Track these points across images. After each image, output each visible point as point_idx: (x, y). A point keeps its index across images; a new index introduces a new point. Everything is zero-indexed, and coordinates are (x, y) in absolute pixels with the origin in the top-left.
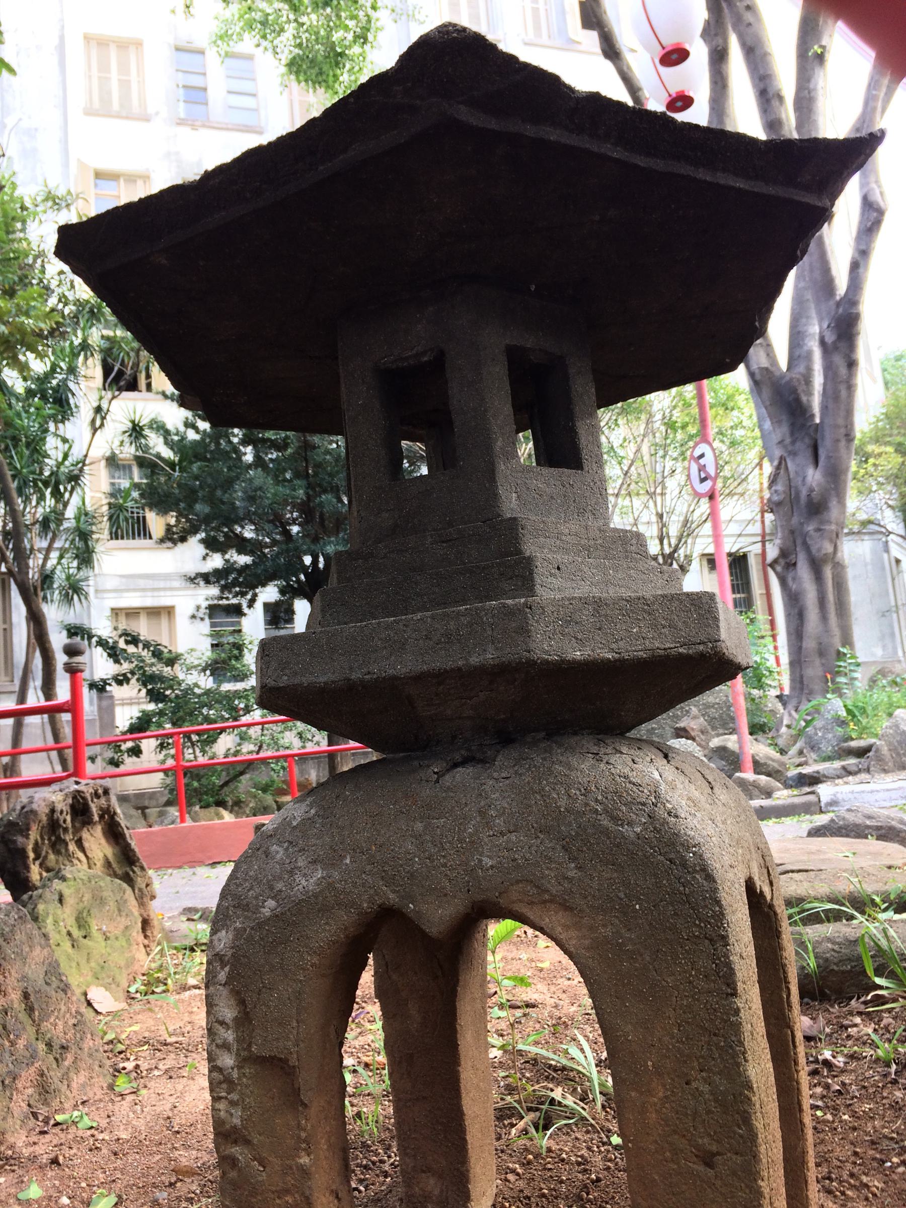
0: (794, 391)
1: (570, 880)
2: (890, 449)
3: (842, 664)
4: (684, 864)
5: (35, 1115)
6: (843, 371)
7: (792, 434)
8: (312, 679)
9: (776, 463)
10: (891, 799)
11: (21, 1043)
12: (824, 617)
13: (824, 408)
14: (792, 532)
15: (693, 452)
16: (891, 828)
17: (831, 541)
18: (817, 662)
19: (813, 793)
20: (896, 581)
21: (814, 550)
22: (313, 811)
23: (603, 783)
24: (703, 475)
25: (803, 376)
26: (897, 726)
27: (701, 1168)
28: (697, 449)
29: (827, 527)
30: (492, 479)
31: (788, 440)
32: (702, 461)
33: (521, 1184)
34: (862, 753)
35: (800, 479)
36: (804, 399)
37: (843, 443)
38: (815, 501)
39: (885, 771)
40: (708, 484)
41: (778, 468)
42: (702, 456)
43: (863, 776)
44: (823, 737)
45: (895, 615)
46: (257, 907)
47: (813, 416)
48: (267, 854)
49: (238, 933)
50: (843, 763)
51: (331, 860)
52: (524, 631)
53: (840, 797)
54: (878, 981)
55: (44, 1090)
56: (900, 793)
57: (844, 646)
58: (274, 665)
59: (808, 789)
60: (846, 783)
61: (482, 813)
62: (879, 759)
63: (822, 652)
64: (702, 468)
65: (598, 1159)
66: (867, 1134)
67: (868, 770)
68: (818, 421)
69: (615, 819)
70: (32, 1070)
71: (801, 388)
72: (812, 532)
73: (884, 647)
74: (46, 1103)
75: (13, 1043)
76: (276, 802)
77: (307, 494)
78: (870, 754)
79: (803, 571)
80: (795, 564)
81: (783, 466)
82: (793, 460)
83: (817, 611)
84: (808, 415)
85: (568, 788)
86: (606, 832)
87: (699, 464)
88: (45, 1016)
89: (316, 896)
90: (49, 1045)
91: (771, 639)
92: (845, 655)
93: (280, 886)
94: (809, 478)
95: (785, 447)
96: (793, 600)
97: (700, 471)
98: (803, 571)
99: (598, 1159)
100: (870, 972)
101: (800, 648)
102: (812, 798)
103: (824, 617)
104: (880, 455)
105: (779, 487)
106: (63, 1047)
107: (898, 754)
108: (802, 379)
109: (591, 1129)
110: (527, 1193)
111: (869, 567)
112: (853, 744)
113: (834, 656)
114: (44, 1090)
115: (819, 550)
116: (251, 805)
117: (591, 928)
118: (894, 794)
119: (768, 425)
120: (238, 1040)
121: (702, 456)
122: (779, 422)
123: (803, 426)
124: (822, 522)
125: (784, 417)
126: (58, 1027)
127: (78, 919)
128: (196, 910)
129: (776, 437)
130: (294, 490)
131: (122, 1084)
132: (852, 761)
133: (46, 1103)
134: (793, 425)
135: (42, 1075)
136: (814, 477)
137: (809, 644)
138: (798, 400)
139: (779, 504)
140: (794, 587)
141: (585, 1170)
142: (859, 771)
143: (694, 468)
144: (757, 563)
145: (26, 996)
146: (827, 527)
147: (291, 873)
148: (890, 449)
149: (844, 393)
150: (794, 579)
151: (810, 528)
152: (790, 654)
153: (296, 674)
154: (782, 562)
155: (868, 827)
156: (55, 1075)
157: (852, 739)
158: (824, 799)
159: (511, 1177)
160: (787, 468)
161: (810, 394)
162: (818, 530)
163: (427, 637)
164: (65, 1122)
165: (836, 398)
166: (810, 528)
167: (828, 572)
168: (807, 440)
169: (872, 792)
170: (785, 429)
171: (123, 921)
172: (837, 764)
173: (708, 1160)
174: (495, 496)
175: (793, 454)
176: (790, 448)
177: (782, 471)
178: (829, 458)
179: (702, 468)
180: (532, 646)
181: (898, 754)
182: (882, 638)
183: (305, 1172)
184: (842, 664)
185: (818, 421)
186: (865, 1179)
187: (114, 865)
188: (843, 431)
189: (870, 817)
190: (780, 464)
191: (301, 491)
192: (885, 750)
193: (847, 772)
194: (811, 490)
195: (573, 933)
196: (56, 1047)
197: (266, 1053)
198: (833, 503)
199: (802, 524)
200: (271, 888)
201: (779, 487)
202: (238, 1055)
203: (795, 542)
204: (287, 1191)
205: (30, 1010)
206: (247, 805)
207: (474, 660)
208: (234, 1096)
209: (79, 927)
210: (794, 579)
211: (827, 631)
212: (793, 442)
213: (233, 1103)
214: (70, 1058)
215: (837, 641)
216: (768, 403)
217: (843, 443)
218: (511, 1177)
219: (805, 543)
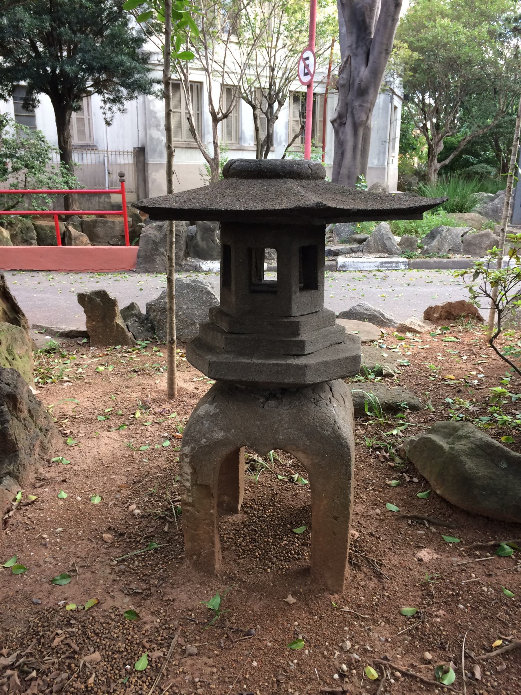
0: (363, 15)
1: (307, 445)
2: (406, 45)
3: (359, 185)
4: (342, 445)
5: (43, 459)
6: (392, 8)
7: (357, 43)
8: (227, 378)
9: (345, 59)
10: (370, 267)
11: (32, 431)
12: (354, 157)
13: (377, 30)
14: (347, 104)
15: (302, 54)
16: (375, 316)
17: (366, 113)
18: (346, 181)
19: (334, 260)
20: (392, 125)
21: (356, 117)
22: (218, 410)
23: (319, 416)
24: (306, 71)
25: (369, 4)
26: (380, 231)
27: (333, 520)
28: (305, 53)
29: (365, 105)
30: (290, 302)
31: (354, 46)
32: (307, 62)
33: (251, 494)
34: (361, 241)
35: (356, 72)
36: (367, 20)
37: (383, 55)
38: (362, 88)
39: (370, 253)
40: (308, 78)
41: (346, 63)
42: (307, 59)
43: (360, 254)
44: (344, 230)
45: (387, 144)
46: (199, 441)
47: (370, 33)
48: (202, 424)
49: (193, 449)
50: (351, 246)
51: (227, 429)
52: (304, 374)
53: (347, 263)
54: (368, 413)
55: (43, 448)
56: (375, 264)
57: (361, 175)
58: (213, 371)
59: (332, 258)
60: (351, 257)
61: (280, 421)
62: (368, 246)
63: (349, 177)
64: (306, 66)
65: (275, 485)
66: (361, 476)
67: (362, 251)
68: (372, 37)
69: (322, 429)
70: (38, 441)
71: (367, 13)
72: (357, 107)
73: (379, 159)
74: (45, 453)
75: (29, 432)
76: (33, 224)
77: (51, 25)
78: (365, 243)
79: (348, 128)
80: (345, 124)
81: (349, 62)
82: (355, 59)
83: (351, 153)
84: (368, 32)
85: (308, 416)
86: (320, 433)
87: (305, 63)
88: (38, 418)
89: (221, 440)
90: (41, 429)
91: (321, 149)
92: (361, 180)
93: (208, 435)
94: (361, 73)
95: (352, 50)
96: (340, 144)
97: (305, 68)
98: (348, 128)
99: (275, 485)
100: (366, 410)
101: (339, 172)
102: (334, 263)
103: (354, 157)
104: (400, 48)
105: (344, 75)
106: (46, 430)
107: (378, 245)
108: (368, 7)
109: (271, 473)
110: (254, 497)
111: (381, 111)
112: (358, 236)
113: (355, 179)
114: (43, 448)
115: (359, 118)
116: (19, 226)
117: (312, 460)
118: (372, 265)
119: (344, 30)
120: (192, 479)
121: (307, 59)
122: (352, 33)
123: (364, 38)
124: (363, 101)
125: (354, 31)
126: (41, 422)
127: (8, 350)
128: (42, 328)
129: (348, 43)
130: (43, 22)
131: (70, 441)
132: (355, 246)
133: (45, 453)
134: (358, 37)
135: (42, 442)
136: (364, 72)
137: (344, 171)
138: (364, 21)
139: (343, 86)
140: (342, 137)
141: (272, 490)
142: (358, 251)
143: (302, 65)
144: (321, 102)
145: (29, 411)
146: (365, 105)
147: (212, 432)
148: (406, 45)
149: (390, 23)
150: (343, 132)
151: (357, 104)
152: (333, 175)
153: (221, 375)
154: (338, 121)
155: (365, 314)
156: (46, 441)
157: (357, 233)
158: (339, 264)
159: (247, 492)
160: (351, 64)
161: (371, 18)
162: (361, 106)
163: (270, 371)
164: (57, 461)
165: (385, 25)
166: (357, 104)
167: (361, 132)
168: (364, 48)
169: (362, 262)
170: (354, 38)
171: (25, 348)
172: (348, 246)
173: (336, 518)
174: (290, 308)
175: (356, 55)
176: (354, 51)
177: (348, 66)
178: (374, 62)
179: (306, 66)
180: (306, 379)
181: (378, 245)
182: (379, 154)
183: (212, 515)
184: (359, 185)
185: (372, 37)
186: (361, 495)
187: (8, 313)
188: (385, 47)
189: (366, 310)
190: (347, 60)
191: (48, 24)
192: (372, 243)
193: (352, 251)
194: (361, 81)
195: (306, 460)
196: (44, 430)
197: (202, 484)
198: (371, 91)
199: (353, 100)
200: (205, 436)
201: (344, 75)
202: (191, 483)
203: (347, 110)
204: (206, 519)
205: (32, 416)
206: (17, 226)
207: (286, 381)
208: (190, 494)
209: (9, 354)
210: (343, 132)
211: (354, 165)
212: (357, 48)
213: (189, 496)
214: (49, 434)
215: (358, 171)
216: (347, 19)
217: (383, 55)
218: (247, 492)
219: (352, 112)
